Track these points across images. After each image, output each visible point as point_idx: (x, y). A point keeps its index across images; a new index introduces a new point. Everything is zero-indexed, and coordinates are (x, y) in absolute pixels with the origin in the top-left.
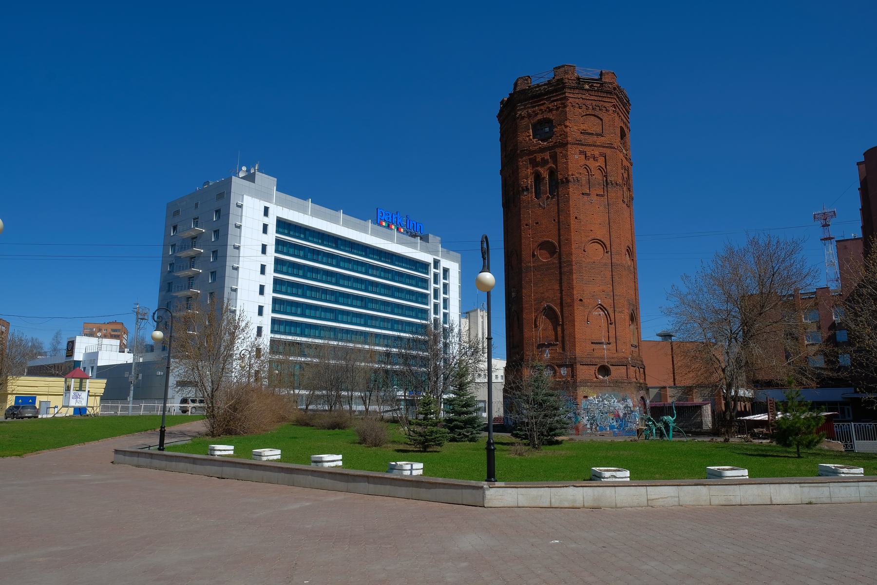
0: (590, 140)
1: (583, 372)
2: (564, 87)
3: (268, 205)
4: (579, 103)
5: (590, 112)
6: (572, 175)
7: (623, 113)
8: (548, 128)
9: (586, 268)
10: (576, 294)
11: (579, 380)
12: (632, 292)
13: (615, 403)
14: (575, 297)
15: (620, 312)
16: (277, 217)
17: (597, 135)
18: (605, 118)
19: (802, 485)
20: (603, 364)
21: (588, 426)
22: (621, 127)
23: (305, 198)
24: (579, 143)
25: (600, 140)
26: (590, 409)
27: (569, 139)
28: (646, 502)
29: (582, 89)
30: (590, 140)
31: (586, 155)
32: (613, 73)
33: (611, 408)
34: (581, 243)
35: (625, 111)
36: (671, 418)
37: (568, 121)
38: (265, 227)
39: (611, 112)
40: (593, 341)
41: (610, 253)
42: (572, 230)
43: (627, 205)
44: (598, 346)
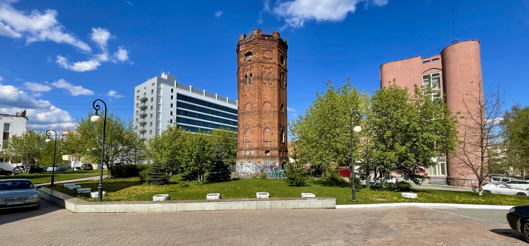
3: (173, 88)
19: (219, 202)
20: (267, 150)
21: (260, 173)
28: (148, 210)
38: (172, 97)
44: (266, 143)
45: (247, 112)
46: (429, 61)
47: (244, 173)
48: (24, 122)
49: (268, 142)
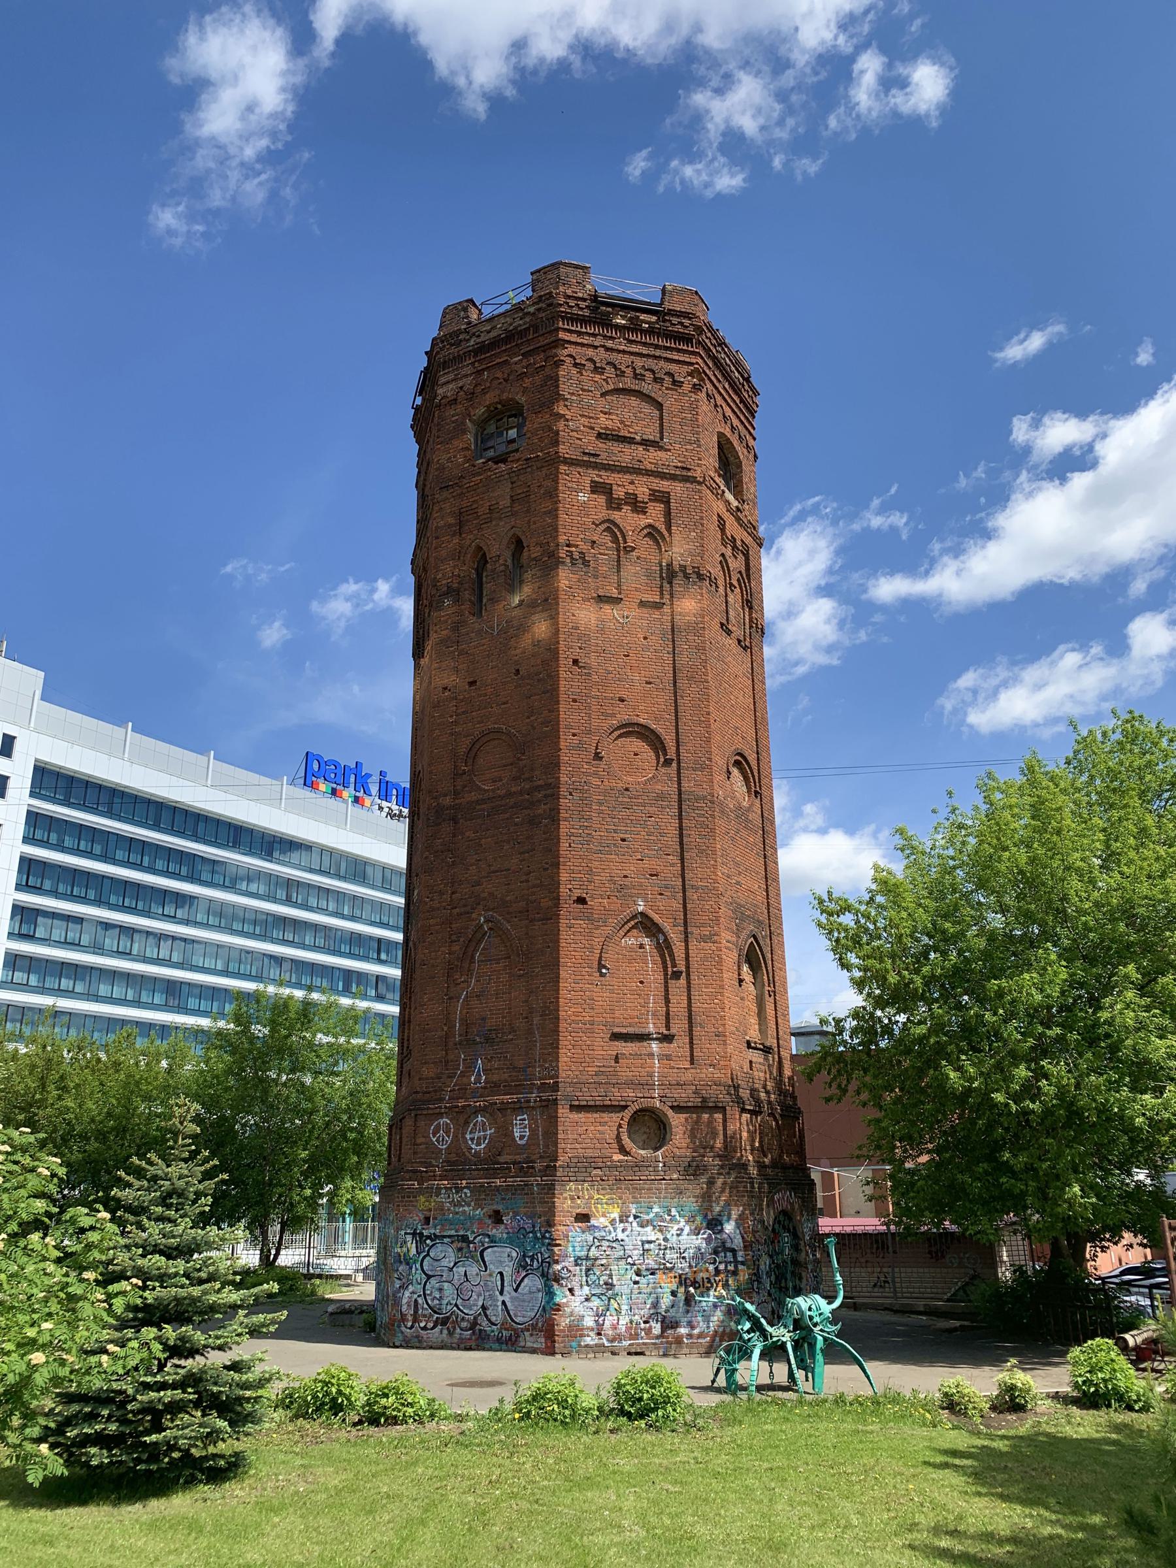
0: (626, 455)
1: (581, 1130)
2: (553, 319)
4: (596, 359)
5: (629, 383)
6: (568, 546)
7: (734, 407)
8: (515, 430)
9: (601, 804)
10: (568, 883)
11: (562, 1160)
12: (757, 885)
13: (684, 1237)
14: (563, 890)
15: (704, 939)
16: (36, 760)
17: (645, 443)
18: (670, 401)
20: (646, 1103)
22: (721, 435)
23: (120, 722)
24: (590, 462)
25: (652, 458)
26: (596, 1259)
27: (562, 449)
29: (606, 323)
30: (626, 455)
31: (611, 494)
32: (696, 293)
33: (668, 1257)
34: (589, 732)
35: (741, 406)
36: (822, 1302)
37: (561, 403)
39: (687, 387)
40: (616, 1030)
41: (674, 765)
42: (562, 697)
43: (739, 641)
45: (483, 801)
46: (616, 1037)
47: (444, 1322)
48: (725, 1120)
49: (643, 1037)
